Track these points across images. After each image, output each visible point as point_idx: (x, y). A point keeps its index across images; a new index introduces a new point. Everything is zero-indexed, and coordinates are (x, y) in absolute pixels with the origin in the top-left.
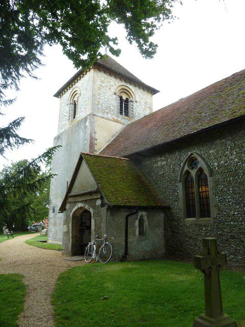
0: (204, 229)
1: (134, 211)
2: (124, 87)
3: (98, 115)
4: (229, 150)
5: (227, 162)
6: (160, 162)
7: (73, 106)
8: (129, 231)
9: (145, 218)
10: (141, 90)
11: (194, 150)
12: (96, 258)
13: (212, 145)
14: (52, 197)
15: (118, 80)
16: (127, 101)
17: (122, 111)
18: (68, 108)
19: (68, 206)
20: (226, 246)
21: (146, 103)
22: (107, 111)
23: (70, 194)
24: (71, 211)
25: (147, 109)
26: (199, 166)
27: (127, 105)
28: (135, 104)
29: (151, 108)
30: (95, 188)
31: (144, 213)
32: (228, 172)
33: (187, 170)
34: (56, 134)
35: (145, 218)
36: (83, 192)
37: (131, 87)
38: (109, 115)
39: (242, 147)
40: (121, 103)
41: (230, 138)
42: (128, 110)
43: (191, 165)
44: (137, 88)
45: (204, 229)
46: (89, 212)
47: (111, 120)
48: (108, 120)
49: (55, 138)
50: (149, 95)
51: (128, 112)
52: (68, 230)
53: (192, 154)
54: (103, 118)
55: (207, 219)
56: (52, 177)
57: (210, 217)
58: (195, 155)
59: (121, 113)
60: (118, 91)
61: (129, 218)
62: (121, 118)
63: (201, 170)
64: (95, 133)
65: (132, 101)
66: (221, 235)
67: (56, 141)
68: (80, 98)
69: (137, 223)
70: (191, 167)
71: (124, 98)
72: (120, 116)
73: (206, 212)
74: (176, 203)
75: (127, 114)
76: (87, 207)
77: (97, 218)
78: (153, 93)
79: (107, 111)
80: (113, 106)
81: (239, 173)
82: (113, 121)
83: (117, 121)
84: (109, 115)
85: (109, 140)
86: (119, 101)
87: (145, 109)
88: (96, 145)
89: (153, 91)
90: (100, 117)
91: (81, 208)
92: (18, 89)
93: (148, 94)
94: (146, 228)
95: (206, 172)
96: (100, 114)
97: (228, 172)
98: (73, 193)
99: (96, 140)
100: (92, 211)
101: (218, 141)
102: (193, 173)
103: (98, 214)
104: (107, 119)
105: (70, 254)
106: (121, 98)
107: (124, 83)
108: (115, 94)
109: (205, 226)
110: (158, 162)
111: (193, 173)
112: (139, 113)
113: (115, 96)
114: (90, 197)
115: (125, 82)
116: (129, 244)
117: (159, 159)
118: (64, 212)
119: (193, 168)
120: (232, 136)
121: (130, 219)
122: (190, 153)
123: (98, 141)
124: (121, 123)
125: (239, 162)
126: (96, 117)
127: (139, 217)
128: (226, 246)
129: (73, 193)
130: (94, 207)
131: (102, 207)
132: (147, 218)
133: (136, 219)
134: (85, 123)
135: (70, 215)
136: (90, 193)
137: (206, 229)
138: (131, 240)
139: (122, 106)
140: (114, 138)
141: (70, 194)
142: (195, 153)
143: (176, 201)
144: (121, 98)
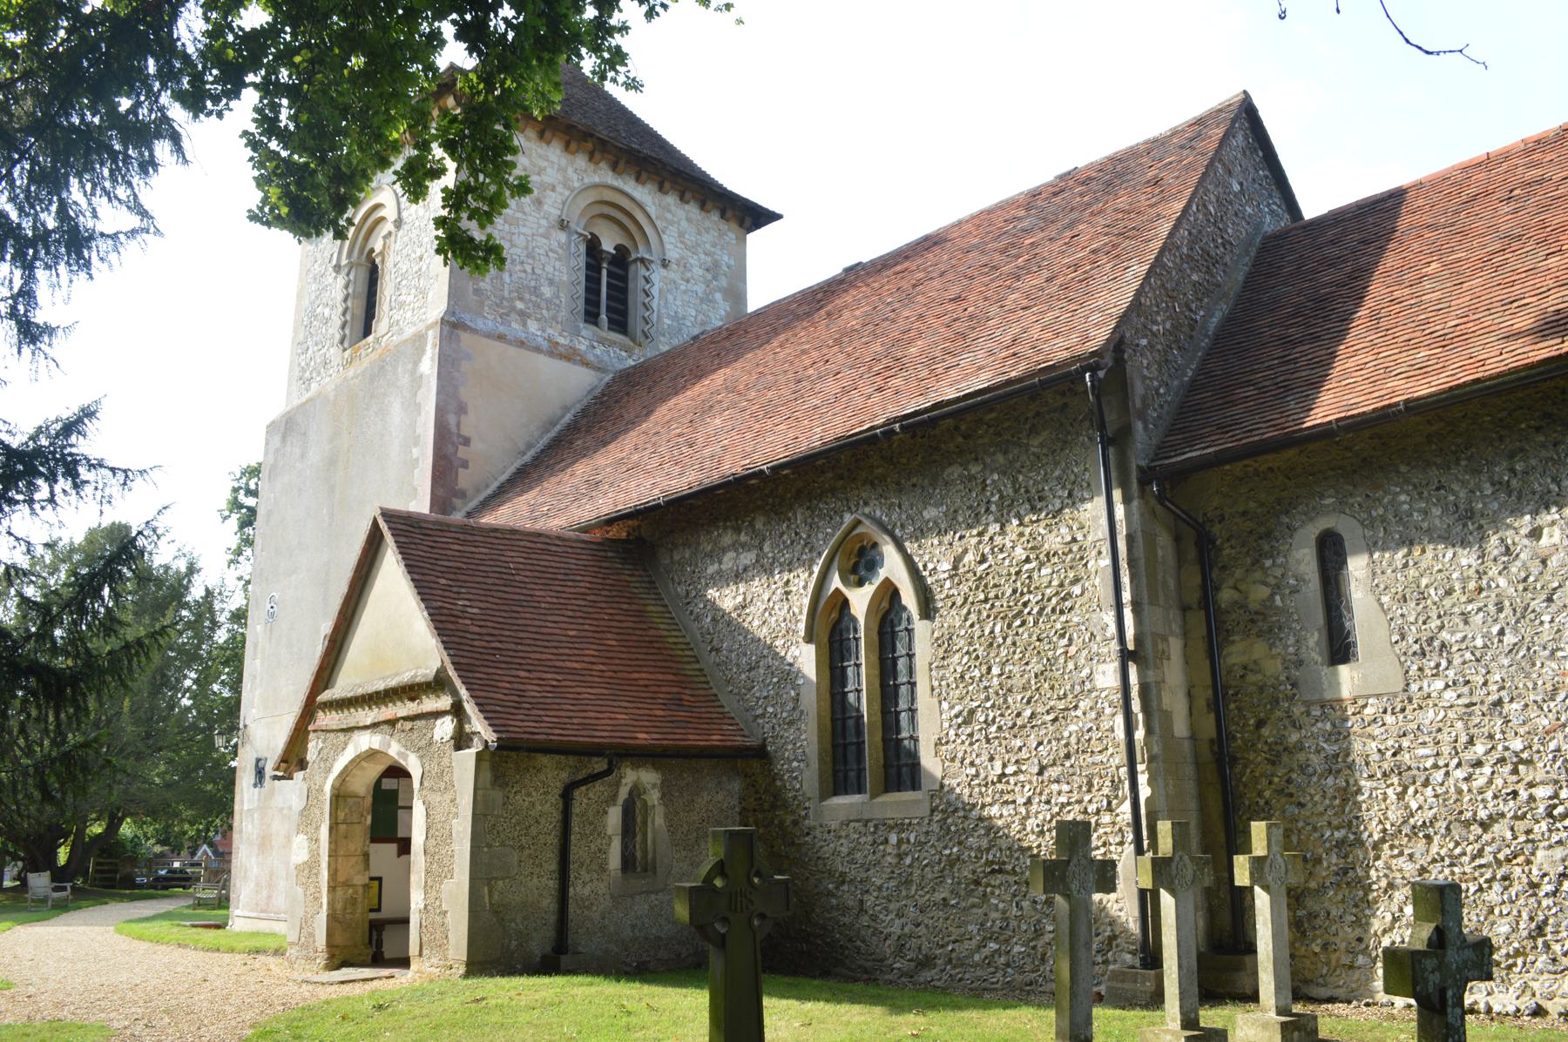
0: (893, 839)
1: (599, 765)
2: (609, 196)
3: (480, 324)
4: (993, 508)
5: (983, 560)
6: (731, 554)
7: (362, 275)
8: (577, 851)
9: (654, 797)
10: (692, 209)
11: (866, 504)
12: (92, 603)
13: (933, 485)
14: (251, 711)
15: (581, 161)
16: (621, 259)
17: (598, 305)
18: (341, 281)
19: (313, 747)
20: (973, 906)
21: (713, 269)
22: (520, 305)
23: (325, 696)
24: (329, 770)
25: (718, 296)
26: (882, 573)
27: (624, 279)
28: (658, 275)
29: (737, 293)
30: (427, 671)
31: (648, 777)
32: (986, 600)
33: (837, 590)
34: (276, 407)
35: (654, 797)
36: (381, 686)
37: (644, 194)
38: (533, 326)
39: (1041, 499)
40: (593, 268)
41: (1000, 458)
42: (625, 302)
43: (854, 570)
44: (671, 200)
45: (893, 839)
46: (407, 775)
47: (538, 350)
48: (522, 351)
49: (272, 428)
50: (730, 232)
51: (624, 313)
52: (315, 855)
53: (858, 523)
54: (501, 337)
55: (907, 795)
56: (1479, 558)
57: (920, 788)
58: (868, 528)
59: (591, 317)
60: (578, 212)
61: (576, 793)
62: (589, 340)
63: (890, 593)
64: (462, 409)
65: (642, 260)
66: (953, 862)
67: (277, 439)
68: (396, 245)
69: (614, 816)
70: (852, 578)
71: (608, 246)
72: (588, 331)
73: (904, 769)
74: (790, 734)
75: (620, 323)
76: (394, 750)
77: (435, 798)
78: (748, 221)
79: (520, 305)
80: (551, 282)
81: (1025, 604)
82: (551, 354)
83: (570, 356)
84: (533, 326)
85: (530, 446)
86: (582, 261)
87: (707, 299)
88: (465, 465)
89: (754, 216)
90: (488, 336)
91: (372, 755)
92: (91, 277)
93: (724, 226)
94: (654, 841)
95: (909, 599)
96: (488, 322)
97: (986, 600)
98: (343, 685)
99: (466, 442)
100: (413, 765)
101: (955, 471)
102: (860, 600)
103: (440, 779)
104: (521, 344)
105: (321, 960)
106: (593, 246)
107: (608, 177)
108: (563, 225)
109: (900, 827)
110: (724, 550)
111: (860, 600)
112: (676, 318)
113: (563, 237)
114: (409, 708)
115: (614, 167)
116: (572, 908)
117: (727, 539)
118: (299, 775)
119: (860, 583)
120: (1005, 453)
121: (583, 799)
122: (848, 518)
123: (477, 446)
124: (586, 364)
125: (1027, 560)
126: (465, 337)
127: (623, 793)
128: (973, 906)
129: (343, 685)
130: (425, 749)
131: (458, 747)
132: (663, 796)
133: (612, 799)
134: (416, 363)
135: (321, 790)
136: (411, 691)
137: (900, 841)
138: (587, 891)
139: (598, 293)
140: (552, 434)
141: (325, 696)
142: (868, 516)
143: (791, 723)
144: (593, 246)
